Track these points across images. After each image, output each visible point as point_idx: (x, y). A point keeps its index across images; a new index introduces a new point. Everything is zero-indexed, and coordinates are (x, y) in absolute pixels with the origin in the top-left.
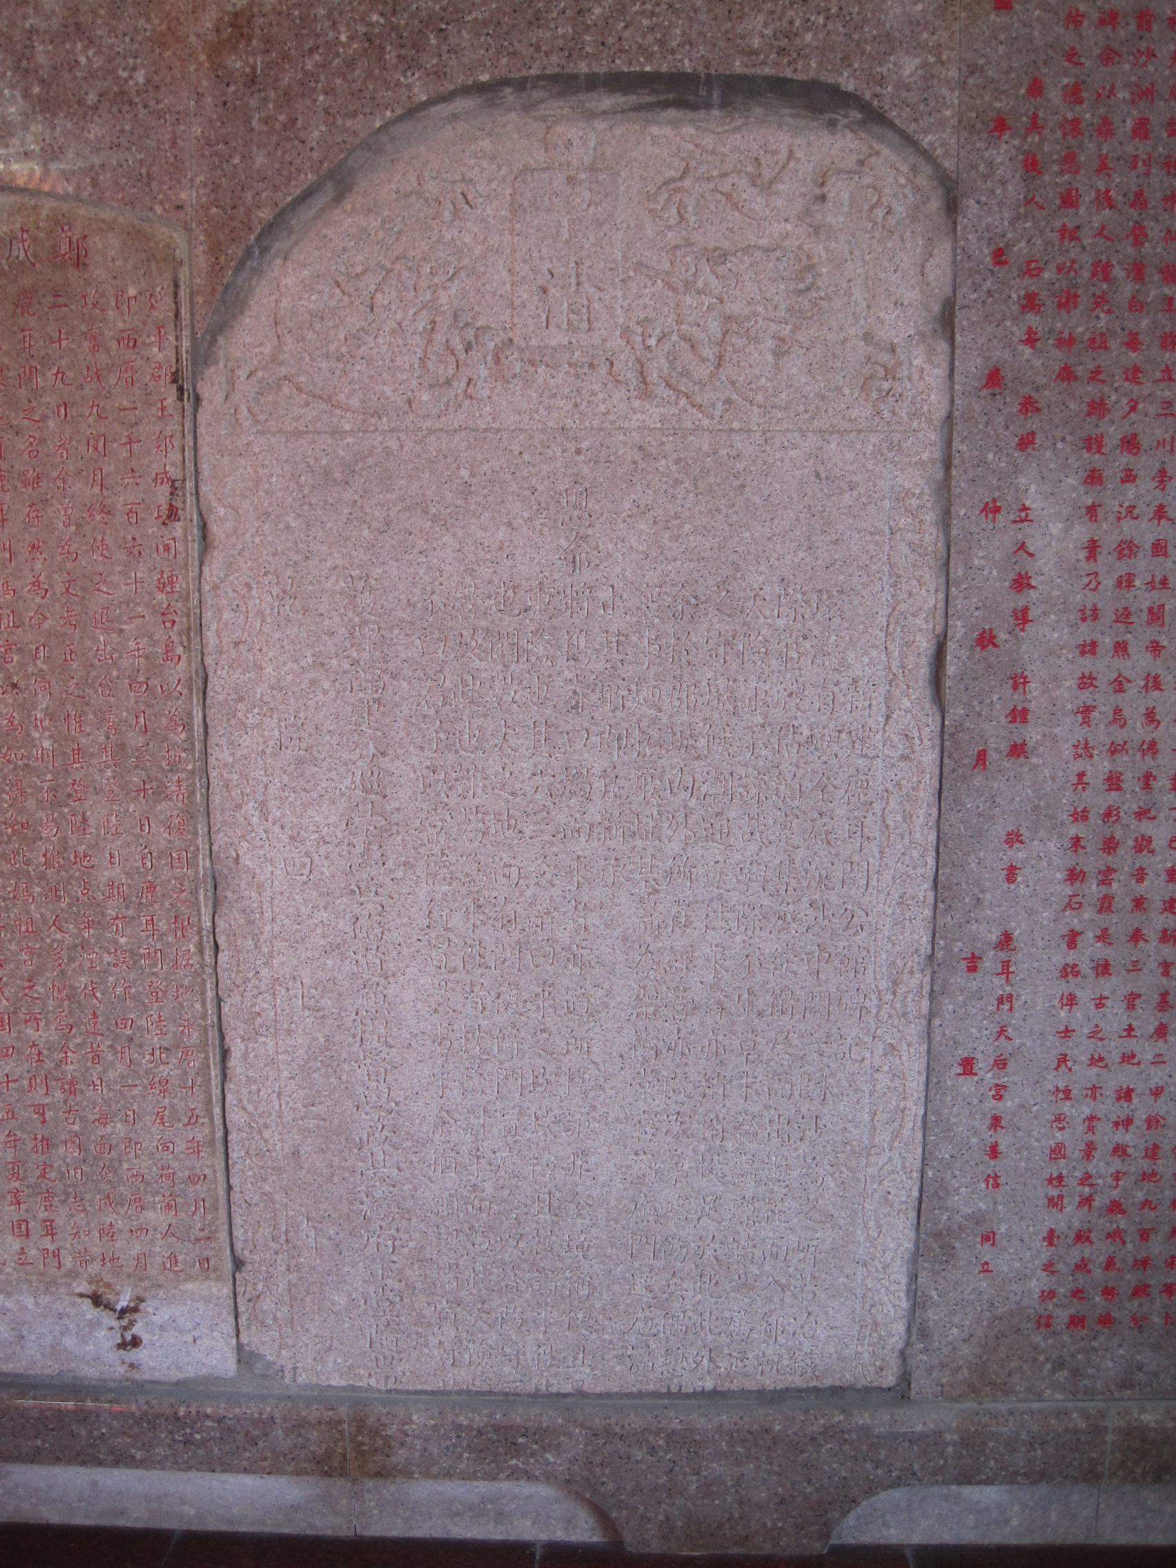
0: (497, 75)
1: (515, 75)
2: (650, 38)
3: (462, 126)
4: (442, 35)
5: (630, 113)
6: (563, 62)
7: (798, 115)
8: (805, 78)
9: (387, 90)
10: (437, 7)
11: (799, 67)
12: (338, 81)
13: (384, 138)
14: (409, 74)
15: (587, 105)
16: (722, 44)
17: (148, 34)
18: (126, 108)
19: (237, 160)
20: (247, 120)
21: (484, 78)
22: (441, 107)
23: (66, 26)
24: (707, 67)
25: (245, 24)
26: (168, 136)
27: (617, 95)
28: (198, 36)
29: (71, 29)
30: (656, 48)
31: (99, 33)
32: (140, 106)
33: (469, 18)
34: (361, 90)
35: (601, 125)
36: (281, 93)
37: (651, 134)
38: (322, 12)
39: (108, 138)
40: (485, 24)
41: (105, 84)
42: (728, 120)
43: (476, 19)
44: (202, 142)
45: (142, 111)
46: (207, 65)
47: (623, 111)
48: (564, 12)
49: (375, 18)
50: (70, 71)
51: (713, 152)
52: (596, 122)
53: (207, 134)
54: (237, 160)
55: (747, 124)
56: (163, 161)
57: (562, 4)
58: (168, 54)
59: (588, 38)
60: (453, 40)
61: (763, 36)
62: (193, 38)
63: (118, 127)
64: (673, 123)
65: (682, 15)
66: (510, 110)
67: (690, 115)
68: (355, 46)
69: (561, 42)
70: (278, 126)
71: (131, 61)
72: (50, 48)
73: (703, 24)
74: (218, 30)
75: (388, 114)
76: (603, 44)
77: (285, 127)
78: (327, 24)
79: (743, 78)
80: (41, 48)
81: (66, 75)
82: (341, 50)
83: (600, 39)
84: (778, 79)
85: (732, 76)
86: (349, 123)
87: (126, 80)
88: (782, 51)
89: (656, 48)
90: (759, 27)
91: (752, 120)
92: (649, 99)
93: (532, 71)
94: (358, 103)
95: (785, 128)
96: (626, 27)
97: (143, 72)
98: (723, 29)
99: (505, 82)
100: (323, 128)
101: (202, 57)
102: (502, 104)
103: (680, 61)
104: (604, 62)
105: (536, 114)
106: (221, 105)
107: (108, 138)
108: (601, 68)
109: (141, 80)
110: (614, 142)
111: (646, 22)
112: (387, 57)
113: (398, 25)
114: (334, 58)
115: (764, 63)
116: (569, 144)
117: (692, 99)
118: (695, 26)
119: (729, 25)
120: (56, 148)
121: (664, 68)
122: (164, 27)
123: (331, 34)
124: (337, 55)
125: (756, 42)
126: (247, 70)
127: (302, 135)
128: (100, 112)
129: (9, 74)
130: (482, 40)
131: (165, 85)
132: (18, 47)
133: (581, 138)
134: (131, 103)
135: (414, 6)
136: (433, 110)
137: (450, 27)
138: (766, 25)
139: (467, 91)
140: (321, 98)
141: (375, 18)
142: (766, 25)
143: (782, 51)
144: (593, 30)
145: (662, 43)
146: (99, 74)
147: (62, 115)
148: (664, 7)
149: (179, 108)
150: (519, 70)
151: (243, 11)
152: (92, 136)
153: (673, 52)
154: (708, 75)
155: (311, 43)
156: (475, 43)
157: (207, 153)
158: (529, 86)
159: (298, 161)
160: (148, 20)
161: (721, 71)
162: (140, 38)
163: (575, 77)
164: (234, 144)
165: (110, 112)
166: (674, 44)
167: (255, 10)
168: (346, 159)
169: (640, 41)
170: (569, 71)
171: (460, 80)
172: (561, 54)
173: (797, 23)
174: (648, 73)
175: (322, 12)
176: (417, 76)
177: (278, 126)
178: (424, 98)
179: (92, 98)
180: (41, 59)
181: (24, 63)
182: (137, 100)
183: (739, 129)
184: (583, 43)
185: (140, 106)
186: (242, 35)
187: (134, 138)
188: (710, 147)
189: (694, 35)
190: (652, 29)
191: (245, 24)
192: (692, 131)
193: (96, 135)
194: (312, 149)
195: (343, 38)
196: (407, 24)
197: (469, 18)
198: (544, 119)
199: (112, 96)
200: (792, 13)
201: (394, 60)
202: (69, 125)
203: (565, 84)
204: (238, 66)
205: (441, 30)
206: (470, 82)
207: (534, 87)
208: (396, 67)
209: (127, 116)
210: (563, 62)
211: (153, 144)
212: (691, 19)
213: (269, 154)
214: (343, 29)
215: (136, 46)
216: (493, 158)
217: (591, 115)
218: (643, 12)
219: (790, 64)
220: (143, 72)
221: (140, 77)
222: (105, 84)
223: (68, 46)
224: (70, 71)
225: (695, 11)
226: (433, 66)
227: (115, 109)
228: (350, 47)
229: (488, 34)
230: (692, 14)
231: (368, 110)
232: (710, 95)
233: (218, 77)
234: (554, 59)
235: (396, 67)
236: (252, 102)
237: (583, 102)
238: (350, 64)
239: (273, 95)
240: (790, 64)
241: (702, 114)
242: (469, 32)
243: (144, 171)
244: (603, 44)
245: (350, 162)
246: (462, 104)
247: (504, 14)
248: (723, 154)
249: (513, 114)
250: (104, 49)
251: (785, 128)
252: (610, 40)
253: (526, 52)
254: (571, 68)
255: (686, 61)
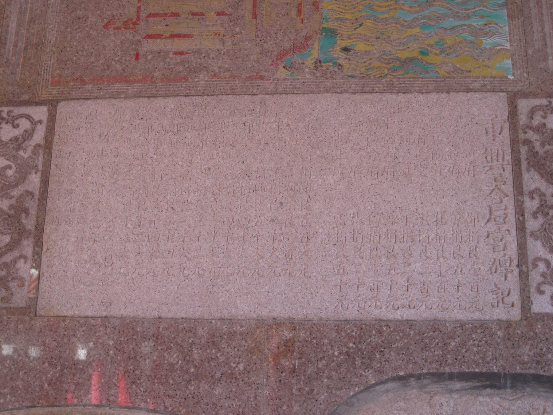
0: (407, 372)
1: (416, 372)
2: (478, 356)
3: (390, 395)
4: (382, 353)
5: (469, 390)
6: (438, 367)
7: (547, 392)
8: (549, 374)
9: (356, 378)
10: (380, 341)
11: (546, 370)
12: (334, 373)
13: (354, 400)
14: (367, 371)
15: (449, 387)
16: (511, 359)
17: (246, 347)
18: (234, 380)
19: (285, 408)
20: (291, 390)
21: (402, 373)
22: (381, 386)
23: (208, 342)
24: (504, 370)
25: (291, 345)
26: (253, 395)
27: (463, 382)
28: (269, 350)
29: (211, 344)
30: (480, 361)
31: (223, 346)
32: (240, 380)
33: (394, 346)
34: (344, 378)
35: (456, 396)
36: (307, 377)
37: (479, 401)
38: (326, 341)
39: (224, 394)
40: (402, 349)
41: (225, 369)
42: (514, 394)
43: (397, 346)
44: (269, 398)
45: (241, 382)
46: (272, 363)
47: (466, 390)
48: (438, 344)
49: (351, 345)
50: (208, 362)
51: (509, 409)
52: (453, 394)
53: (271, 395)
54: (285, 408)
55: (523, 396)
56: (250, 406)
57: (437, 341)
58: (254, 357)
59: (449, 356)
60: (387, 356)
61: (529, 355)
62: (266, 351)
63: (229, 389)
64: (490, 395)
65: (492, 346)
66: (413, 388)
67: (497, 391)
68: (342, 357)
69: (436, 358)
70: (305, 393)
71: (237, 359)
72: (200, 351)
73: (501, 350)
74: (278, 348)
75: (357, 389)
76: (456, 359)
77: (308, 393)
78: (329, 347)
79: (521, 375)
80: (196, 351)
81: (206, 364)
82: (335, 359)
83: (455, 357)
84: (537, 375)
85: (516, 374)
86: (338, 393)
87: (234, 368)
88: (538, 362)
89: (480, 361)
90: (527, 351)
91: (526, 394)
92: (478, 384)
93: (423, 371)
94: (343, 383)
95: (541, 398)
96: (466, 351)
97: (242, 364)
98: (511, 352)
99: (411, 376)
100: (326, 394)
101: (271, 359)
102: (409, 386)
103: (492, 367)
104: (457, 367)
105: (425, 390)
106: (278, 381)
107: (224, 394)
108: (456, 370)
109: (241, 368)
110: (462, 404)
111: (475, 349)
112: (357, 363)
113: (362, 348)
114: (332, 362)
115: (530, 368)
116: (441, 405)
117: (498, 384)
118: (498, 351)
119: (514, 351)
120: (199, 397)
121: (484, 370)
122: (253, 345)
123: (331, 352)
124: (333, 361)
125: (526, 359)
126: (291, 366)
127: (316, 397)
128: (221, 382)
129: (180, 362)
130: (400, 356)
131: (253, 371)
132: (186, 350)
133: (447, 402)
134: (236, 378)
135: (369, 340)
136: (378, 388)
137: (385, 350)
138: (530, 351)
139: (393, 379)
140: (325, 380)
141: (351, 345)
142: (530, 351)
143: (538, 362)
144: (451, 352)
145: (483, 359)
146: (222, 364)
147: (203, 382)
148: (484, 342)
149: (258, 382)
150: (418, 370)
151: (290, 339)
152: (217, 393)
153: (488, 363)
154: (505, 373)
155: (321, 355)
156: (397, 357)
157: (271, 403)
158: (422, 377)
159: (315, 409)
160: (246, 342)
161: (510, 371)
162: (242, 349)
163: (444, 374)
164: (284, 400)
165: (226, 382)
166: (488, 359)
167: (296, 339)
168: (337, 409)
169: (473, 357)
170: (441, 371)
171: (390, 374)
172: (437, 364)
173: (544, 350)
174: (477, 372)
175: (326, 341)
176: (370, 372)
177: (305, 393)
178: (374, 382)
179: (218, 375)
180: (196, 356)
181: (188, 357)
182: (239, 377)
183: (519, 398)
184: (447, 358)
185: (240, 380)
186: (289, 350)
187: (236, 395)
188: (507, 407)
189: (497, 355)
190: (478, 353)
191: (291, 345)
192: (499, 399)
193: (219, 392)
194: (321, 404)
195: (336, 353)
196: (366, 348)
197: (394, 346)
198: (429, 393)
199: (227, 375)
200: (541, 345)
201: (360, 364)
202: (206, 387)
203: (439, 377)
204: (287, 364)
205: (381, 351)
206: (395, 375)
207: (425, 378)
208: (360, 367)
209: (234, 384)
210: (438, 367)
211: (246, 398)
212: (496, 348)
213: (300, 406)
214: (336, 349)
215: (240, 353)
216: (406, 410)
217: (451, 391)
218: (474, 345)
219: (542, 368)
220: (242, 364)
221: (241, 367)
222: (225, 369)
223: (208, 351)
224: (208, 362)
225: (498, 344)
226: (378, 368)
227: (228, 381)
228: (339, 357)
229: (403, 354)
230: (496, 346)
231: (347, 387)
232: (506, 383)
233: (277, 368)
234: (434, 365)
235: (360, 367)
236: (293, 381)
237: (447, 385)
238: (339, 365)
239: (303, 378)
240: (542, 368)
241: (502, 391)
242: (394, 352)
243: (241, 410)
244: (456, 359)
245: (338, 411)
246: (390, 385)
247: (411, 344)
248: (514, 410)
249: (415, 391)
250: (225, 354)
251: (541, 398)
252: (459, 357)
253: (420, 362)
254: (441, 370)
255: (494, 367)
